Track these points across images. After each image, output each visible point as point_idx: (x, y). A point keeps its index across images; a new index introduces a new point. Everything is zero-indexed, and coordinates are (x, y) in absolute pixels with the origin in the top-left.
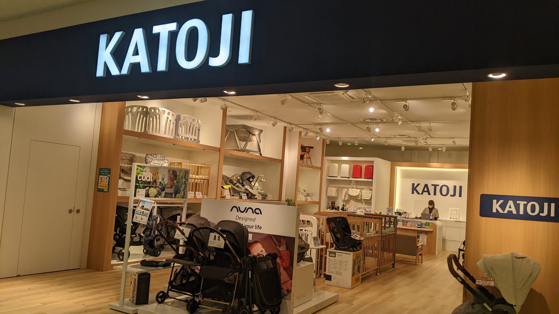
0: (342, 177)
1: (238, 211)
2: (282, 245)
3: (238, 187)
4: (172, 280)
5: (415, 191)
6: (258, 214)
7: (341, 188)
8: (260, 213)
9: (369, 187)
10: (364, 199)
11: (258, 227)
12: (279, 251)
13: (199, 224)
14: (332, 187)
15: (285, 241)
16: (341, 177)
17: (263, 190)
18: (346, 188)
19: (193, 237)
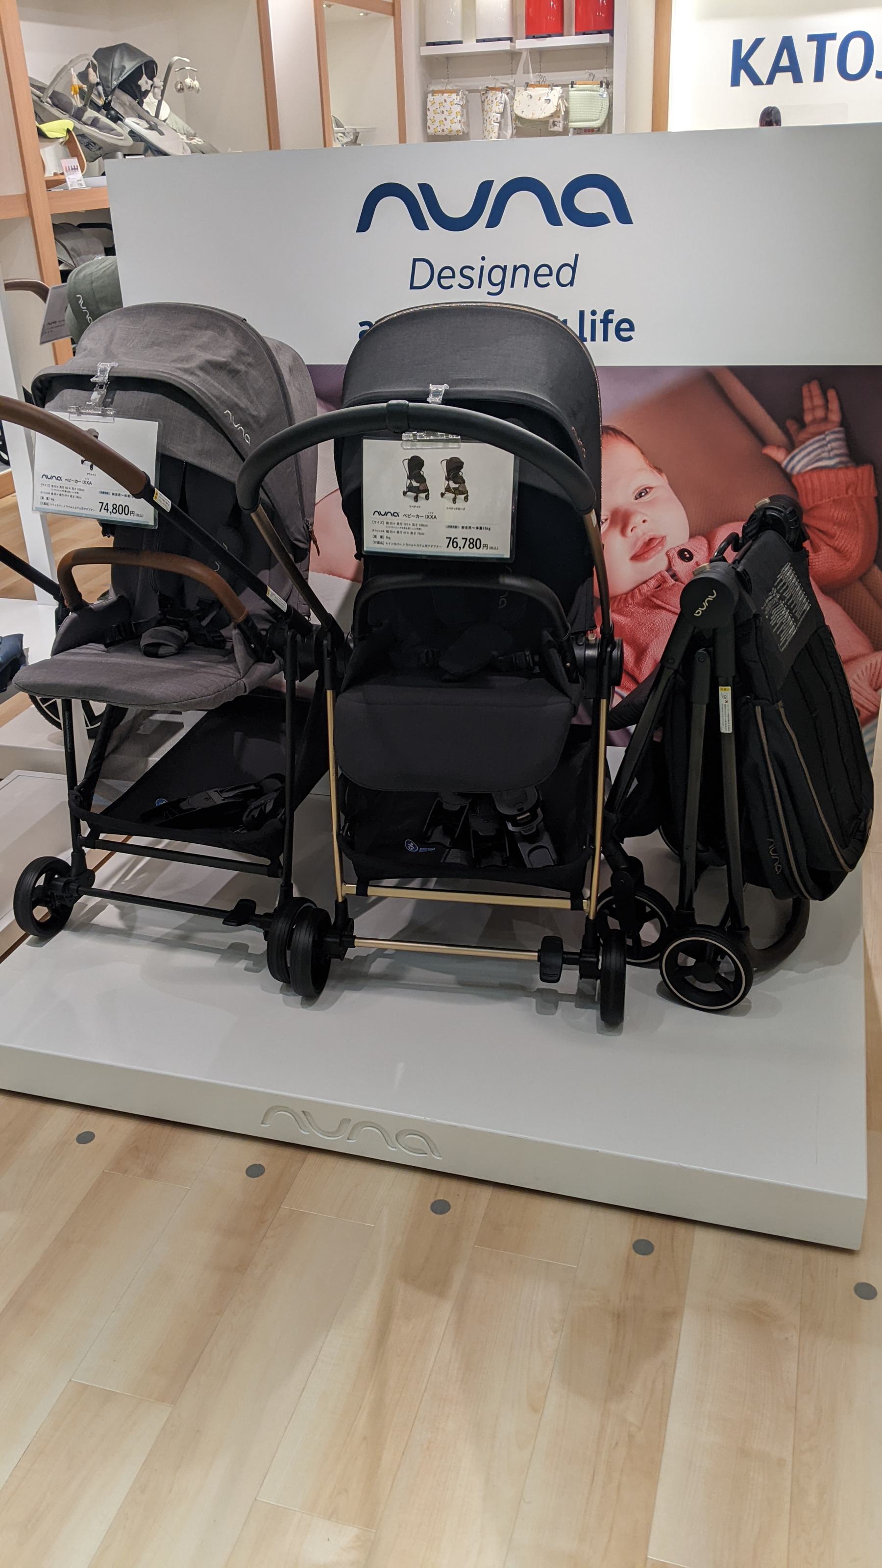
0: (484, 41)
1: (421, 225)
2: (811, 429)
3: (94, 123)
4: (81, 777)
5: (743, 73)
6: (599, 219)
7: (478, 91)
8: (610, 213)
9: (594, 72)
10: (575, 129)
11: (606, 321)
12: (787, 477)
13: (202, 368)
14: (443, 92)
15: (834, 405)
16: (478, 41)
17: (195, 136)
18: (501, 89)
19: (254, 508)
